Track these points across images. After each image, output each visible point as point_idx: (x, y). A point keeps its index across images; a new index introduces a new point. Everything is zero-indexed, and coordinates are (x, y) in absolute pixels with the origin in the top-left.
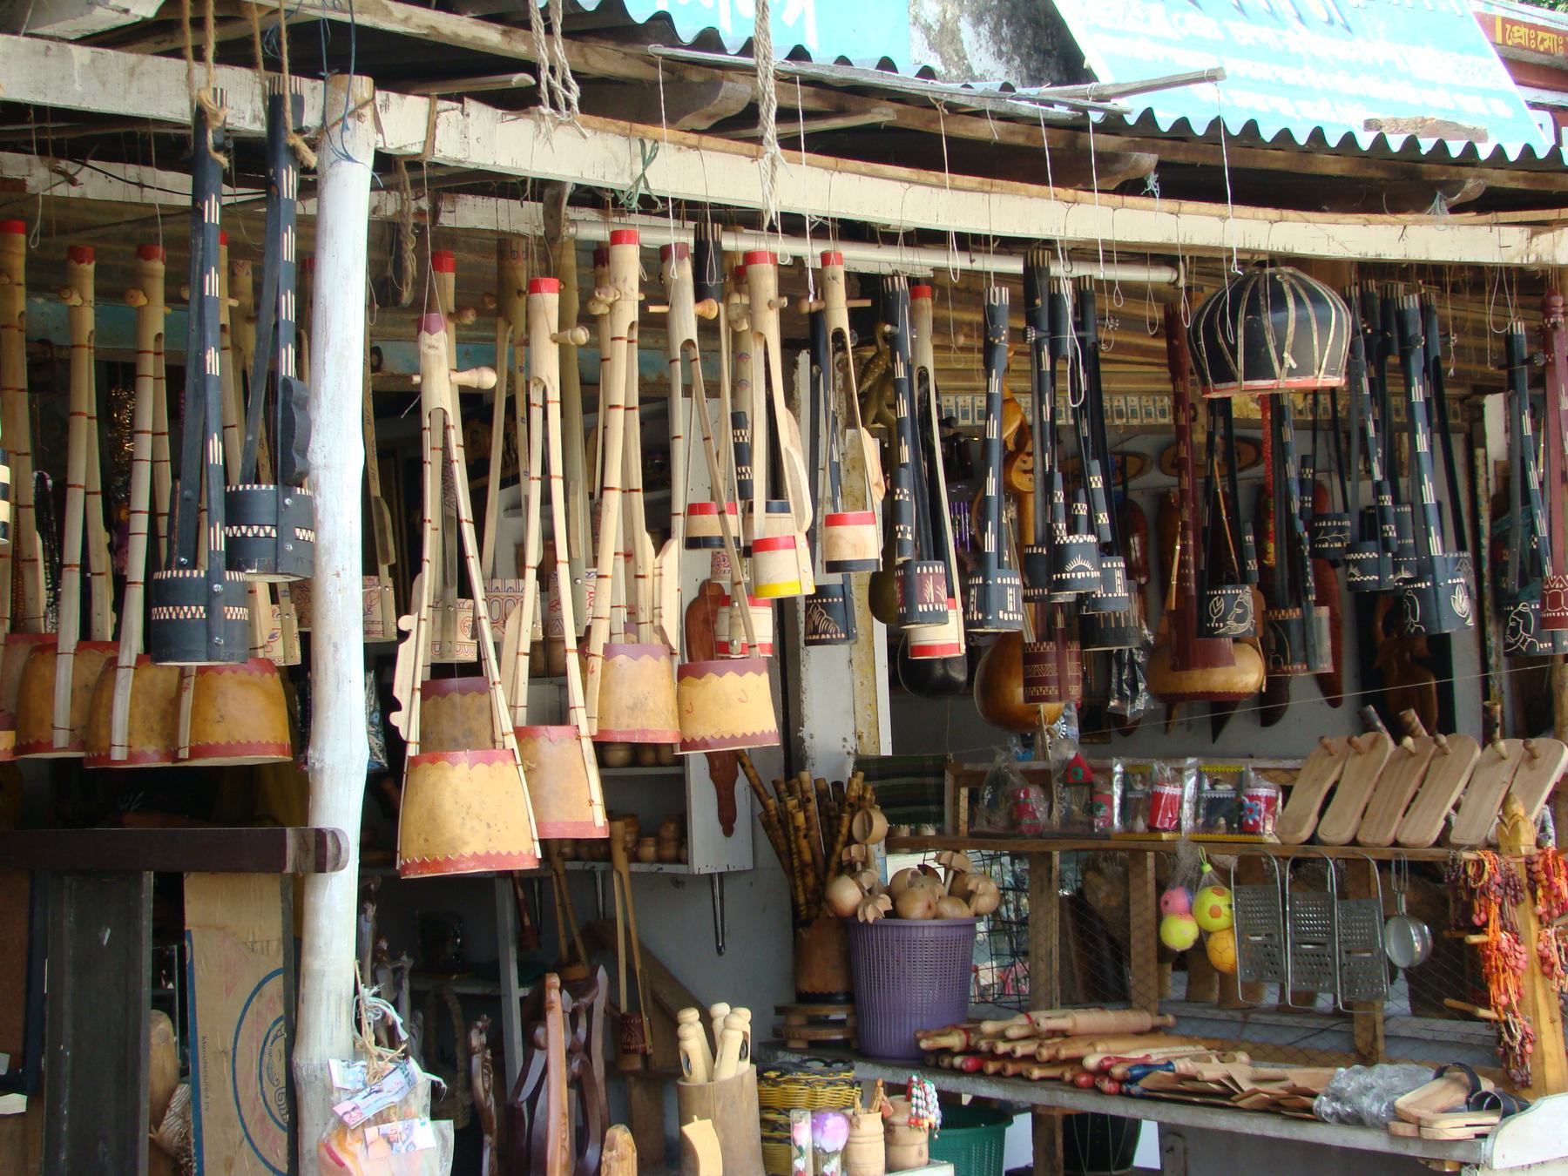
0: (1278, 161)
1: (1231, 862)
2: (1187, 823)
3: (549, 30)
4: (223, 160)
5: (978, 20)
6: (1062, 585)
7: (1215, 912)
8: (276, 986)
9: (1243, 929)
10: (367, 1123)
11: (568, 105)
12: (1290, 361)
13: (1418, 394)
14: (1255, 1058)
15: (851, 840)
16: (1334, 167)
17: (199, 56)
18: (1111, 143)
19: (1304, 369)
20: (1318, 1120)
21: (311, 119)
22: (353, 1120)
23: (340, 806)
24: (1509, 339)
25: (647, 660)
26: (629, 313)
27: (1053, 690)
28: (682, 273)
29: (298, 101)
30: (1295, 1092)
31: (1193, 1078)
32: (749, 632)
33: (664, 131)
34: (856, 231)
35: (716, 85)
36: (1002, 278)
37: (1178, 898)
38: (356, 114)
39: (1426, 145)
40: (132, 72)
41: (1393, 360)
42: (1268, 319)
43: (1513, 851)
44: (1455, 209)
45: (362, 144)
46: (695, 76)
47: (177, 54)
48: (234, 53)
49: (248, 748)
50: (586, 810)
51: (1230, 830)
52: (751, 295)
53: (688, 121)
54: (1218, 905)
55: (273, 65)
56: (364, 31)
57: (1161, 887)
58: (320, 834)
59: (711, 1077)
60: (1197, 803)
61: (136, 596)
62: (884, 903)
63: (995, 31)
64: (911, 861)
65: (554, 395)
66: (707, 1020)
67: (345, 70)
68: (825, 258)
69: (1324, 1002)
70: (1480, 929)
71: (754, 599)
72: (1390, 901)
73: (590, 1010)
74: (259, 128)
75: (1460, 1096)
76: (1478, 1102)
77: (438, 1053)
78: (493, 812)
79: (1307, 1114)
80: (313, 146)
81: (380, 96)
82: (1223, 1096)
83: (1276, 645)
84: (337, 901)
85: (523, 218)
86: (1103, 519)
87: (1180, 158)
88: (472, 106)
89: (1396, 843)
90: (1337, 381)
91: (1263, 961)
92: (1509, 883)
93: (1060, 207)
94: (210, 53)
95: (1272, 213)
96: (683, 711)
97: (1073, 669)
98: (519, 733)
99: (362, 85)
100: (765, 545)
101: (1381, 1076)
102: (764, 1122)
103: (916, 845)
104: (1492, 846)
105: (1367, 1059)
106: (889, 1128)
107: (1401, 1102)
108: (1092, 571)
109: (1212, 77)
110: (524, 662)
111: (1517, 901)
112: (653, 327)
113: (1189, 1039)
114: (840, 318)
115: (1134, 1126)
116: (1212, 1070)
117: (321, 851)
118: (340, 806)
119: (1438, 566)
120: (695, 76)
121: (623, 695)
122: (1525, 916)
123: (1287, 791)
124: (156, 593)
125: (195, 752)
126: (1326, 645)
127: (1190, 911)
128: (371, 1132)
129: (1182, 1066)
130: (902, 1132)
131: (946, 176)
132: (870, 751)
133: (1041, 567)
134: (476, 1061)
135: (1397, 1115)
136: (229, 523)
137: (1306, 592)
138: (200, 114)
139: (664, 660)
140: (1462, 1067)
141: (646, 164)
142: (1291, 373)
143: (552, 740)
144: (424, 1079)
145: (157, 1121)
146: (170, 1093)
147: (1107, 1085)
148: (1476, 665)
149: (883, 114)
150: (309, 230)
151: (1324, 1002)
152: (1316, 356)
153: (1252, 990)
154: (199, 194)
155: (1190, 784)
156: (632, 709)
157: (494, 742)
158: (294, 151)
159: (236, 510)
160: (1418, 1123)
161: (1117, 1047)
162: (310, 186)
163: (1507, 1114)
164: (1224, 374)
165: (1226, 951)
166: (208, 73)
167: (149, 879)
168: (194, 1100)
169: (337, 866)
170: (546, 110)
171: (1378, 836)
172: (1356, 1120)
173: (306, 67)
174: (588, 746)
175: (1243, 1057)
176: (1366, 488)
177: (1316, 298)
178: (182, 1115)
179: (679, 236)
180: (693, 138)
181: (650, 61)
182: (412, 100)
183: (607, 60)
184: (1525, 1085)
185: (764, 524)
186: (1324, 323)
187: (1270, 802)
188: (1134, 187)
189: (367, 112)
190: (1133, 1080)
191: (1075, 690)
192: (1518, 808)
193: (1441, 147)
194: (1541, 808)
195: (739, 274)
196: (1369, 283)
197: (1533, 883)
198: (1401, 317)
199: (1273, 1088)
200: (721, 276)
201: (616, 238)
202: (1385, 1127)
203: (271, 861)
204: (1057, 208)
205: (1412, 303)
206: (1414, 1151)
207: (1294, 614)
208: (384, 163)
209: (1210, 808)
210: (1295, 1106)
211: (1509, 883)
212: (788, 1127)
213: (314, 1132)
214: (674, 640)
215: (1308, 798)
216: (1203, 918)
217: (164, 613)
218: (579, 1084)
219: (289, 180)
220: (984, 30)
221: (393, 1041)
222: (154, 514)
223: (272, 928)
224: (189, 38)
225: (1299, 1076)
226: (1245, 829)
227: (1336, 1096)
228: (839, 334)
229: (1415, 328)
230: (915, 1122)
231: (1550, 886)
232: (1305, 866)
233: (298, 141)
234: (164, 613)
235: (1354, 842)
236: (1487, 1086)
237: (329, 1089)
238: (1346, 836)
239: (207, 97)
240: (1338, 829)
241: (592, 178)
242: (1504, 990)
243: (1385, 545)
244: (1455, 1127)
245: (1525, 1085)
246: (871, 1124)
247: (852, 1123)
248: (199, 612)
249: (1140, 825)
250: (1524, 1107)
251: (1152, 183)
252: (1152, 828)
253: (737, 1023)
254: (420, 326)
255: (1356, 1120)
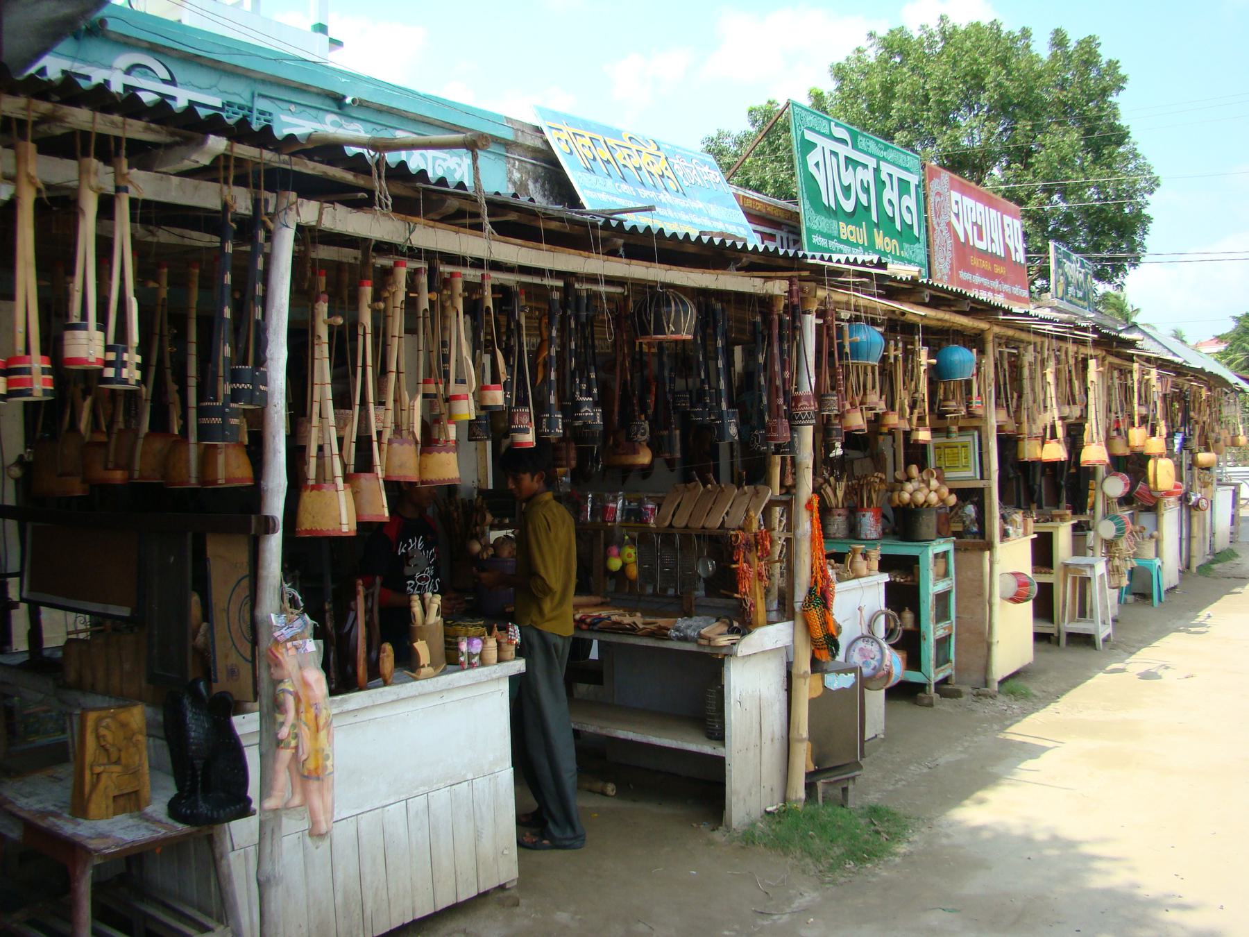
0: (670, 245)
1: (636, 534)
2: (618, 519)
3: (380, 177)
4: (234, 226)
5: (536, 181)
6: (578, 418)
7: (629, 555)
8: (246, 583)
9: (640, 561)
10: (288, 640)
11: (387, 206)
12: (672, 328)
13: (719, 344)
14: (643, 616)
15: (477, 524)
16: (691, 249)
17: (226, 182)
18: (606, 233)
19: (678, 331)
20: (670, 639)
21: (271, 209)
22: (281, 639)
23: (276, 506)
24: (754, 324)
25: (406, 446)
26: (401, 296)
27: (564, 463)
28: (424, 279)
29: (267, 201)
30: (660, 628)
31: (619, 623)
32: (447, 435)
33: (422, 220)
34: (497, 266)
35: (444, 201)
36: (558, 288)
37: (614, 550)
38: (289, 208)
39: (729, 243)
40: (196, 188)
41: (710, 331)
42: (664, 310)
43: (750, 531)
44: (738, 270)
45: (292, 220)
46: (434, 197)
47: (216, 180)
48: (241, 181)
49: (238, 480)
50: (380, 509)
51: (636, 521)
52: (452, 291)
53: (431, 216)
54: (630, 552)
55: (257, 186)
56: (295, 172)
57: (607, 546)
58: (267, 518)
59: (424, 622)
60: (623, 510)
61: (193, 414)
62: (491, 551)
63: (543, 186)
64: (502, 533)
65: (369, 330)
66: (422, 600)
67: (287, 189)
68: (483, 276)
69: (671, 592)
70: (736, 562)
71: (450, 420)
72: (701, 550)
73: (373, 594)
74: (249, 212)
75: (725, 629)
76: (732, 631)
77: (314, 610)
78: (340, 511)
79: (665, 637)
80: (272, 220)
81: (300, 200)
82: (632, 630)
83: (656, 446)
84: (274, 545)
85: (348, 255)
86: (595, 391)
87: (631, 241)
88: (338, 206)
89: (703, 527)
90: (690, 337)
91: (647, 575)
92: (747, 543)
93: (582, 259)
94: (231, 181)
95: (667, 267)
96: (421, 468)
97: (573, 454)
98: (347, 478)
99: (293, 196)
100: (456, 398)
101: (696, 621)
102: (446, 642)
103: (501, 527)
104: (740, 528)
105: (688, 614)
106: (499, 644)
107: (703, 631)
108: (591, 414)
109: (650, 209)
110: (353, 445)
111: (750, 551)
112: (411, 304)
113: (616, 608)
114: (489, 303)
115: (591, 641)
116: (627, 620)
117: (267, 526)
118: (276, 506)
119: (725, 415)
120: (434, 197)
121: (396, 460)
122: (753, 557)
123: (659, 506)
124: (202, 412)
125: (227, 481)
126: (678, 446)
127: (619, 555)
128: (289, 645)
129: (614, 618)
130: (504, 646)
131: (544, 246)
132: (484, 487)
133: (570, 409)
134: (327, 615)
135: (701, 636)
136: (232, 383)
137: (671, 424)
138: (226, 206)
139: (413, 446)
140: (726, 617)
141: (410, 233)
142: (672, 333)
143: (365, 480)
144: (311, 622)
145: (195, 637)
146: (199, 627)
147: (584, 627)
148: (728, 455)
149: (512, 217)
150: (268, 259)
151: (671, 592)
152: (683, 327)
153: (642, 587)
154: (223, 242)
155: (620, 502)
156: (400, 466)
157: (1045, 407)
158: (264, 223)
159: (235, 377)
160: (709, 639)
161: (588, 611)
162: (270, 237)
163: (743, 635)
164: (645, 332)
165: (633, 571)
166: (118, 175)
167: (190, 535)
168: (211, 629)
169: (274, 531)
170: (377, 208)
171: (697, 524)
172: (685, 639)
173: (270, 188)
174: (381, 482)
175: (639, 614)
176: (698, 380)
177: (683, 303)
178: (205, 635)
179: (423, 265)
180: (431, 223)
181: (416, 190)
182: (312, 202)
183: (401, 190)
184: (750, 623)
185: (454, 389)
186: (686, 313)
187: (653, 510)
188: (613, 253)
189: (294, 207)
190: (595, 624)
191: (573, 463)
192: (752, 513)
193: (734, 244)
194: (759, 515)
195: (447, 282)
196: (702, 296)
197: (757, 543)
198: (714, 311)
199: (652, 627)
200: (439, 284)
201: (396, 264)
202: (696, 642)
203: (245, 529)
204: (581, 260)
205: (719, 306)
206: (707, 650)
207: (666, 433)
208: (300, 229)
209: (627, 512)
210: (661, 634)
211: (747, 543)
212: (457, 644)
213: (264, 643)
214: (419, 437)
215: (668, 509)
216: (624, 558)
217: (205, 421)
218: (368, 625)
219: (261, 235)
220: (538, 185)
221: (297, 607)
222: (398, 372)
223: (243, 557)
224: (222, 174)
225: (662, 622)
226: (642, 521)
227: (677, 630)
228: (488, 308)
229: (720, 317)
230: (510, 642)
231: (763, 545)
232: (667, 536)
233: (266, 218)
234: (205, 421)
235: (686, 527)
236: (736, 624)
237: (271, 626)
238: (683, 524)
239: (229, 198)
240: (680, 522)
241: (387, 238)
242: (745, 586)
243: (705, 405)
244: (723, 641)
245: (750, 623)
246: (492, 643)
247: (484, 642)
248: (219, 420)
249: (599, 519)
250: (750, 632)
251: (621, 251)
252: (604, 521)
253: (436, 601)
254: (317, 301)
255: (685, 639)
